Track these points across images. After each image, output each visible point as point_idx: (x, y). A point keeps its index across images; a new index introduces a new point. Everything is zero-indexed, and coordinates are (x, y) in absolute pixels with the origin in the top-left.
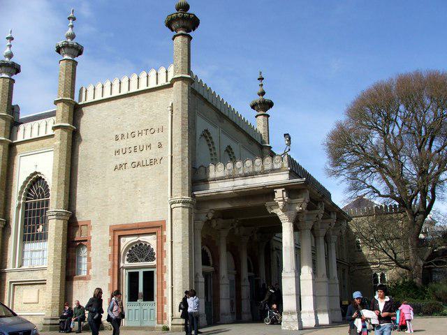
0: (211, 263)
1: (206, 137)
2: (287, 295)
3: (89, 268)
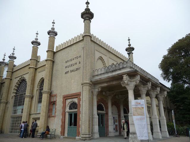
0: (105, 110)
1: (101, 59)
2: (131, 124)
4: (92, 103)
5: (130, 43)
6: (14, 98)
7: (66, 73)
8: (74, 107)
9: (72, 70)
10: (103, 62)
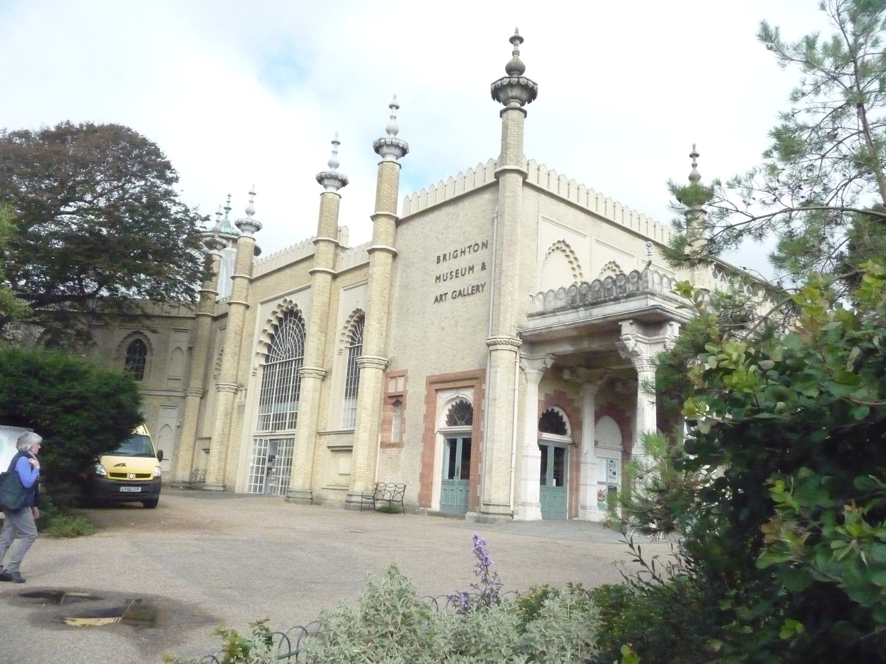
0: (569, 432)
3: (402, 432)
4: (521, 406)
5: (698, 168)
6: (260, 372)
7: (439, 299)
8: (462, 418)
9: (458, 289)
10: (568, 253)
